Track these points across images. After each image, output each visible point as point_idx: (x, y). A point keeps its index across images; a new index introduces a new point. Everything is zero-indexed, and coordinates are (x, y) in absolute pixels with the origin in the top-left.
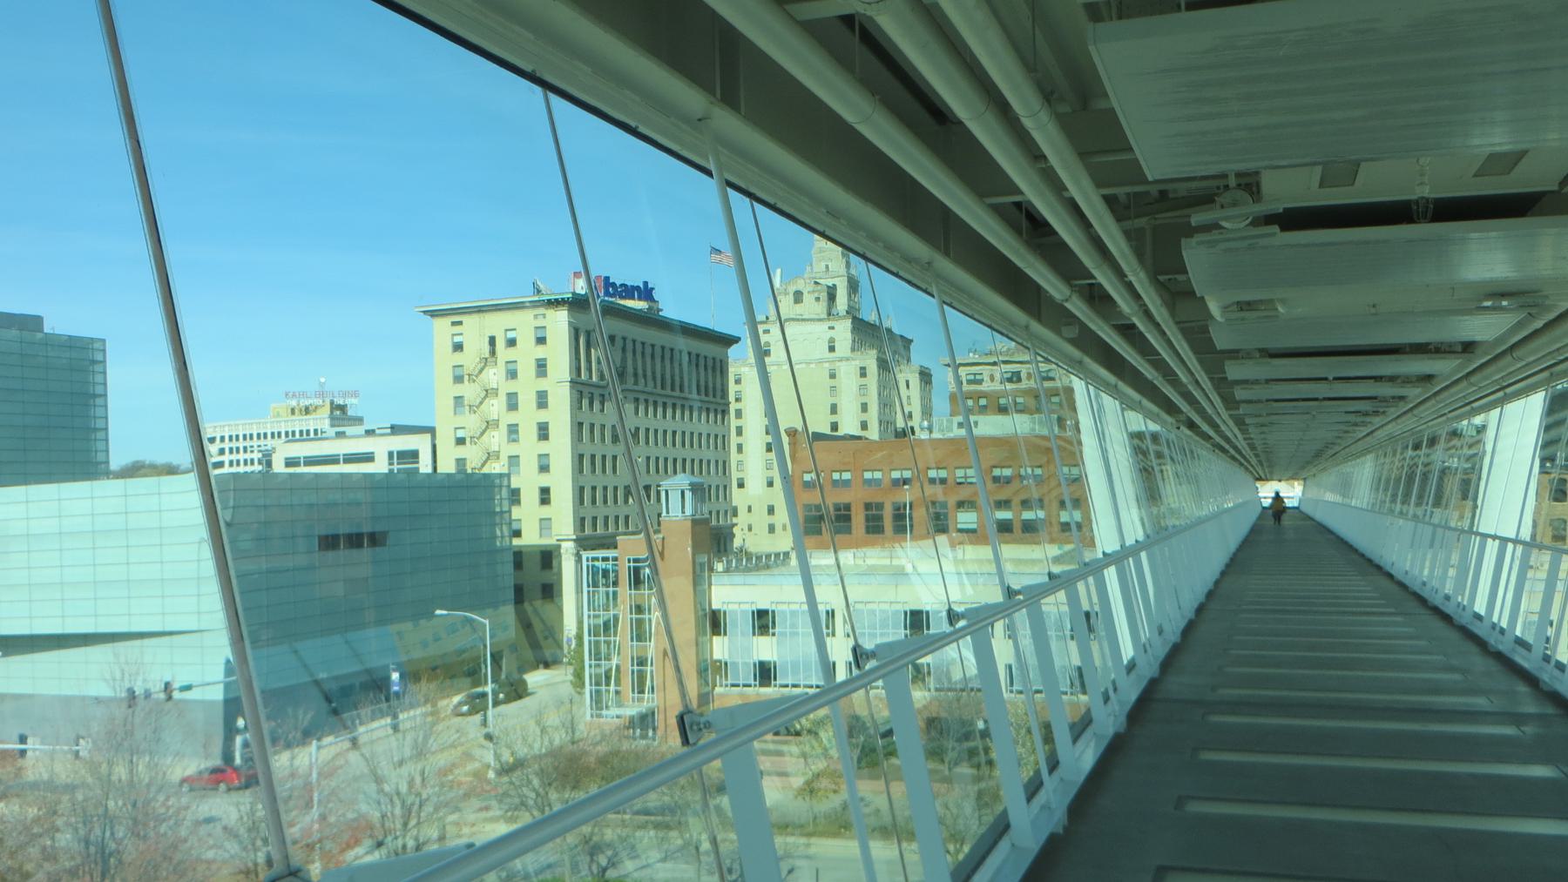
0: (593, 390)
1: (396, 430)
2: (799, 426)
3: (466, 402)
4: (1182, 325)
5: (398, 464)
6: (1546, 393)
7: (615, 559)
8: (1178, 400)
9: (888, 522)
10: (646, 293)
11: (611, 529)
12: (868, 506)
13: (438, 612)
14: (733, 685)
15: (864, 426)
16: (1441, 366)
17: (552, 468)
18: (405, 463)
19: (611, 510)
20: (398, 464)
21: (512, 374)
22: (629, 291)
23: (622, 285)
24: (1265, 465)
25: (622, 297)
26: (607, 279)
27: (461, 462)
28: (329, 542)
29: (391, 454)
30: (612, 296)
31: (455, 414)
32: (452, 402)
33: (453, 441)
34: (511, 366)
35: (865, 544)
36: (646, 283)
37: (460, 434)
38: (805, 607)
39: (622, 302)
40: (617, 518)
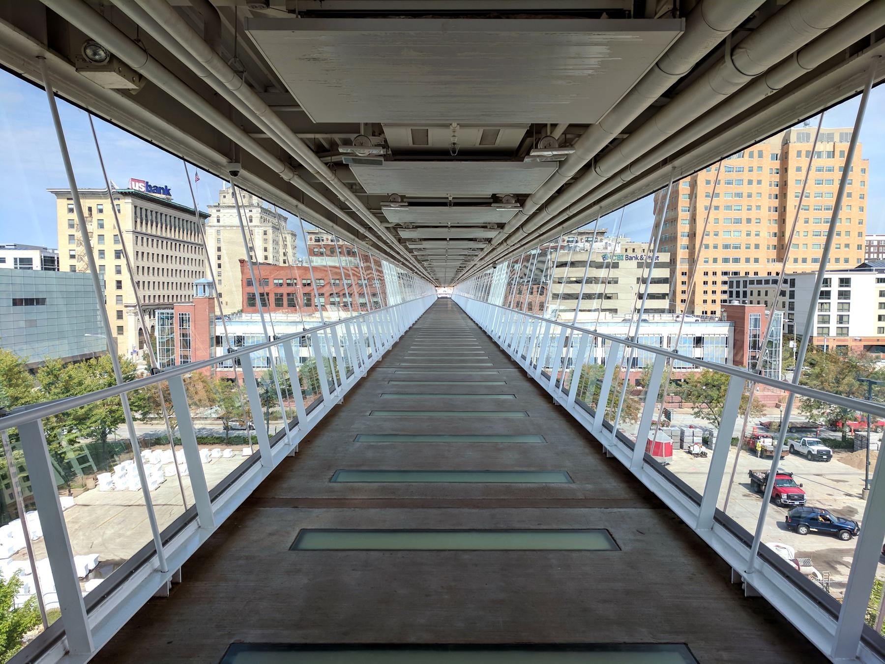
0: (143, 236)
1: (16, 247)
2: (246, 258)
3: (76, 238)
4: (698, 502)
5: (20, 265)
6: (336, 479)
7: (172, 314)
8: (346, 218)
9: (285, 302)
10: (166, 191)
11: (171, 301)
12: (288, 294)
13: (86, 335)
14: (225, 367)
15: (266, 258)
16: (505, 213)
17: (6, 261)
18: (24, 265)
19: (157, 293)
20: (20, 265)
21: (101, 226)
22: (158, 189)
23: (155, 186)
24: (438, 283)
25: (154, 192)
26: (147, 183)
27: (73, 268)
28: (16, 302)
29: (15, 259)
30: (149, 191)
31: (69, 243)
32: (67, 238)
33: (69, 256)
34: (101, 222)
35: (275, 311)
36: (166, 187)
37: (72, 253)
38: (264, 335)
39: (154, 194)
40: (155, 296)
